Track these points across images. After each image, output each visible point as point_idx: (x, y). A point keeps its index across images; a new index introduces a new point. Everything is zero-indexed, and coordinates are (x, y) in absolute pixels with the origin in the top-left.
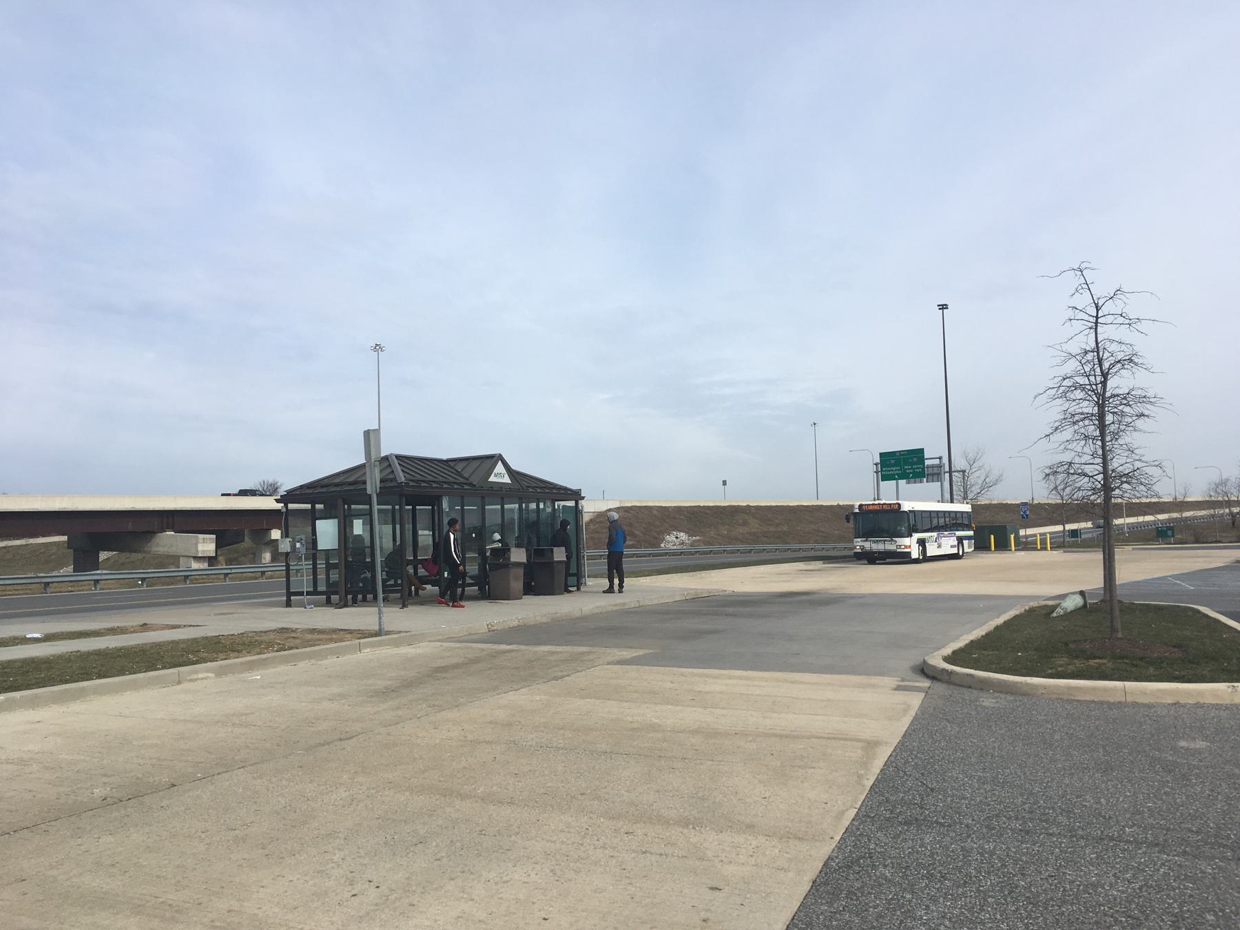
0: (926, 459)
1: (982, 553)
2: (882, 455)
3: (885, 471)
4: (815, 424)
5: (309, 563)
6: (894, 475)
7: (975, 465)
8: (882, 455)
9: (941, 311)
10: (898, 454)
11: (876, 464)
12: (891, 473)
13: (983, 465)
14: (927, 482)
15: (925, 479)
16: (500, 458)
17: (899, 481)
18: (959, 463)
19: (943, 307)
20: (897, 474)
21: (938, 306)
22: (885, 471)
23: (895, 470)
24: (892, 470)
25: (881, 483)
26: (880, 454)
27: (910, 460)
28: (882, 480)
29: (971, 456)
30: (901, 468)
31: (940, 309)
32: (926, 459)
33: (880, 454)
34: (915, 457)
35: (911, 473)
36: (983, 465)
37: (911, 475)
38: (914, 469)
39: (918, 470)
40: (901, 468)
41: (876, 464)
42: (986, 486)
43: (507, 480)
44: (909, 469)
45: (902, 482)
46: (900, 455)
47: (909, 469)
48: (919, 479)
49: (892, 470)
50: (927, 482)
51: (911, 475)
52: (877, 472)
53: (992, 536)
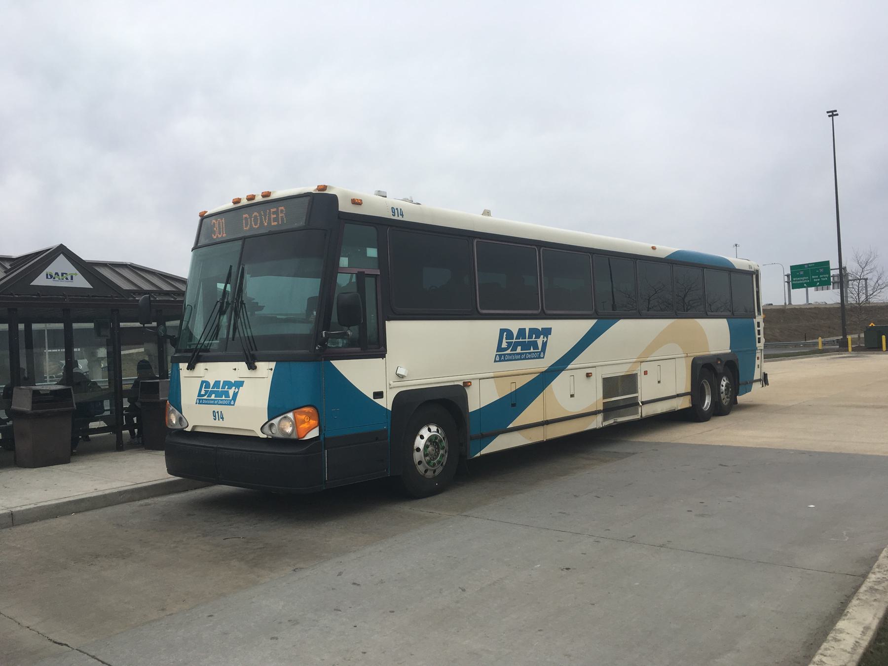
0: (831, 270)
1: (874, 354)
2: (792, 268)
3: (795, 281)
4: (736, 245)
5: (106, 384)
6: (803, 284)
7: (868, 268)
8: (792, 268)
9: (831, 117)
10: (806, 266)
11: (788, 276)
12: (800, 282)
13: (875, 268)
14: (833, 288)
15: (831, 286)
16: (62, 250)
17: (809, 288)
18: (851, 266)
19: (833, 114)
20: (805, 283)
21: (828, 112)
22: (795, 281)
23: (804, 280)
24: (802, 280)
25: (792, 290)
26: (791, 266)
27: (818, 271)
28: (793, 288)
29: (863, 259)
30: (809, 278)
31: (829, 116)
32: (831, 270)
33: (791, 266)
34: (821, 268)
35: (818, 282)
36: (875, 268)
37: (818, 283)
38: (819, 278)
39: (824, 279)
40: (809, 278)
41: (788, 276)
42: (878, 287)
43: (80, 282)
44: (816, 278)
45: (811, 290)
46: (809, 267)
47: (816, 278)
48: (821, 287)
49: (802, 280)
50: (833, 288)
51: (818, 283)
52: (788, 282)
53: (884, 337)
